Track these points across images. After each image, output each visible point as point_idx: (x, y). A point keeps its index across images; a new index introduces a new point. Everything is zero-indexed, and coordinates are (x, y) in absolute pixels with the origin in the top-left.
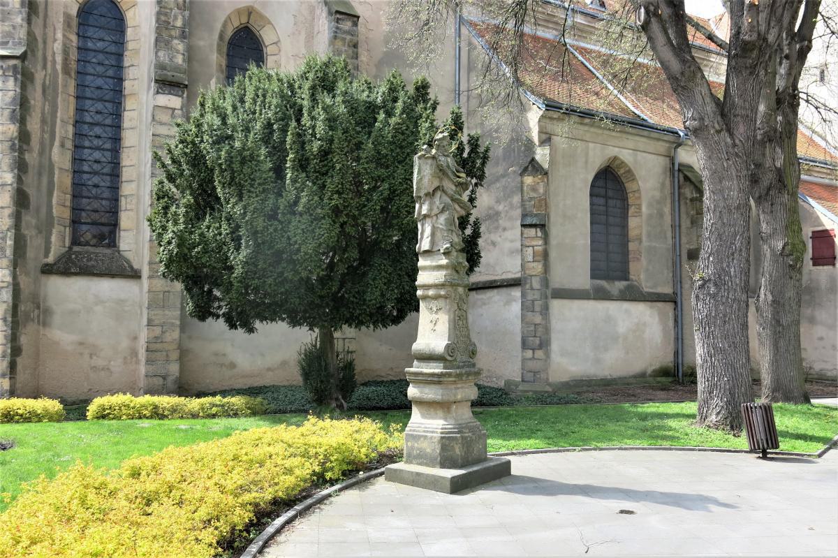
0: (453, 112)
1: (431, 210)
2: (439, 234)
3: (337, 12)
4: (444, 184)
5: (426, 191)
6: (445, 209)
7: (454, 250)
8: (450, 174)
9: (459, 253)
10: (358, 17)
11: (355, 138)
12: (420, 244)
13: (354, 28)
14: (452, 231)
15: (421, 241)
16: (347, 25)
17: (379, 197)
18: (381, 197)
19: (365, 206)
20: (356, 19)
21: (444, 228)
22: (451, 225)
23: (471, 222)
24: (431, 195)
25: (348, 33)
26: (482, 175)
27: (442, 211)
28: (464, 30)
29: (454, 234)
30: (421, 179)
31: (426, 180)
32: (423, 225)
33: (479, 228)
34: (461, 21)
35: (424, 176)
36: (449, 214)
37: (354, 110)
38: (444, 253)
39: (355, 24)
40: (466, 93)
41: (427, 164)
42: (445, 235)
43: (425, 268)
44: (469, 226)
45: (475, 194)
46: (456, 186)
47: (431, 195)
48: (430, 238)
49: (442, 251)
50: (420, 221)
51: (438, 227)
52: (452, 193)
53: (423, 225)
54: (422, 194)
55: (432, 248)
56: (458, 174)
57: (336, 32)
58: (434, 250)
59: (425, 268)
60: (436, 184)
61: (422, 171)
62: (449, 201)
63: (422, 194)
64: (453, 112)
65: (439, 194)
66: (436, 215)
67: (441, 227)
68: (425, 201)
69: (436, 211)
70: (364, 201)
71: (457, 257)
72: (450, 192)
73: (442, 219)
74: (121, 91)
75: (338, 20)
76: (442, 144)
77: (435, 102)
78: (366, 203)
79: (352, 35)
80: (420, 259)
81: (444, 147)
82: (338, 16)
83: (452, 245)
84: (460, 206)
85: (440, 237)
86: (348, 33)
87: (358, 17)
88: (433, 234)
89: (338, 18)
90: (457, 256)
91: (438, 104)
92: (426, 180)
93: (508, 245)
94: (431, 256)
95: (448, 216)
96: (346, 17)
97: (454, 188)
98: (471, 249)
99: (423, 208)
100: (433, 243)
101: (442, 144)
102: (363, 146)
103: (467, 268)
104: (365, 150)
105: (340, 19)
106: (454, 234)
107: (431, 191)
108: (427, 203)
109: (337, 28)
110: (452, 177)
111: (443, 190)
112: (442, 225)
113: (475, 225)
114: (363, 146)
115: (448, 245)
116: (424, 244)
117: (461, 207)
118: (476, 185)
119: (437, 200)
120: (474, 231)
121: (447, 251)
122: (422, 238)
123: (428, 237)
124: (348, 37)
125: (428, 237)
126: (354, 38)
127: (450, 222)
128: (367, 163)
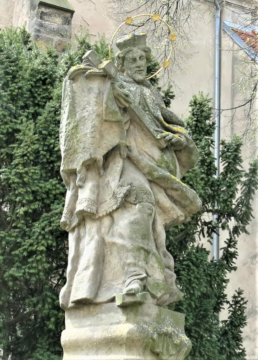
0: (195, 103)
1: (97, 201)
2: (114, 261)
3: (42, 4)
4: (133, 144)
5: (87, 157)
6: (132, 199)
7: (150, 301)
8: (147, 119)
9: (166, 311)
10: (72, 12)
11: (6, 123)
12: (70, 286)
13: (66, 26)
14: (148, 252)
15: (72, 279)
16: (55, 22)
17: (43, 229)
18: (47, 230)
19: (17, 245)
20: (68, 15)
21: (128, 244)
22: (145, 237)
23: (230, 298)
24: (98, 166)
25: (57, 32)
26: (246, 213)
27: (125, 203)
28: (227, 42)
29: (153, 261)
30: (76, 127)
31: (87, 129)
32: (78, 240)
33: (242, 309)
34: (222, 29)
35: (83, 119)
36: (140, 211)
37: (9, 77)
38: (124, 307)
39: (68, 22)
40: (229, 113)
41: (90, 90)
42: (130, 260)
43: (77, 346)
44: (226, 306)
45: (234, 246)
46: (162, 150)
47: (98, 166)
48: (91, 269)
49: (118, 302)
50: (73, 230)
51: (114, 244)
52: (153, 164)
53: (78, 240)
54: (77, 165)
55: (96, 295)
56: (167, 125)
57: (39, 31)
58: (100, 300)
59: (77, 346)
60: (112, 139)
61: (78, 110)
62: (140, 180)
63: (77, 165)
64: (195, 103)
65: (117, 165)
66: (110, 214)
67: (119, 241)
68: (84, 180)
69: (109, 204)
70: (17, 237)
71: (159, 320)
72: (145, 161)
73: (124, 221)
74: (114, 339)
75: (42, 16)
76: (130, 55)
77: (167, 94)
78: (19, 240)
79: (62, 36)
80: (68, 322)
81: (135, 60)
82: (43, 9)
83: (145, 288)
84: (171, 198)
85: (119, 267)
86: (57, 32)
87: (72, 12)
88: (100, 260)
89: (42, 12)
90: (159, 315)
91: (172, 97)
92: (87, 129)
93: (251, 29)
94: (90, 315)
95: (138, 216)
96: (55, 11)
97: (157, 154)
98: (229, 346)
99: (81, 197)
100: (98, 281)
101: (130, 55)
102: (18, 136)
103: (185, 350)
104: (22, 141)
105: (46, 14)
106: (153, 261)
107: (100, 157)
108: (89, 185)
109: (41, 25)
110: (153, 127)
111: (129, 158)
112: (121, 236)
113: (237, 302)
114: (18, 136)
115: (135, 286)
116: (78, 286)
117: (175, 201)
118: (236, 230)
119: (113, 179)
120: (234, 313)
121: (129, 300)
122: (75, 269)
123: (86, 268)
124: (57, 38)
125: (86, 268)
126: (64, 40)
127: (143, 231)
128: (24, 165)
